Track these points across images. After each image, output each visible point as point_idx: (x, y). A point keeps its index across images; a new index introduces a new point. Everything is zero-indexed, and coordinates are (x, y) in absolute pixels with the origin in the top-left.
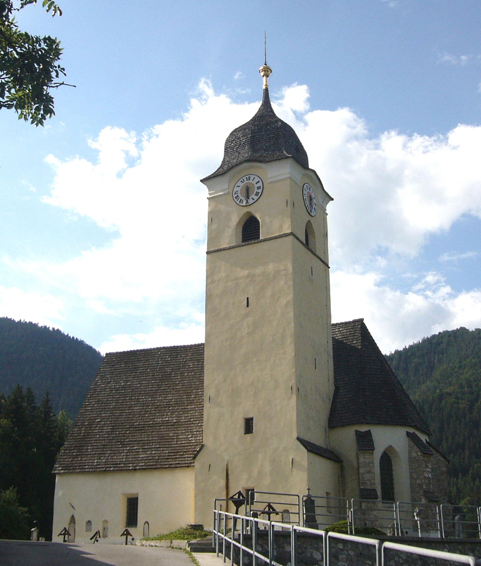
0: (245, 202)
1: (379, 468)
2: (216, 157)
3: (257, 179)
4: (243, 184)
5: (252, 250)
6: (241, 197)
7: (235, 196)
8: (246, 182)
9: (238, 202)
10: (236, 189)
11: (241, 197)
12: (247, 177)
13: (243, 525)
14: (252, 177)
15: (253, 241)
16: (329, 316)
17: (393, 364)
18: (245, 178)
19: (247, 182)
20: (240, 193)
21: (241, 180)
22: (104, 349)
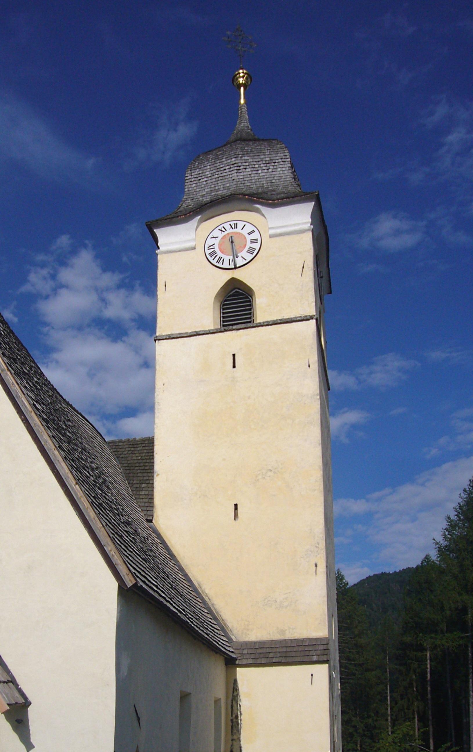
3: (249, 228)
4: (224, 234)
5: (237, 339)
7: (208, 252)
8: (229, 230)
9: (214, 262)
10: (210, 242)
14: (240, 225)
18: (227, 226)
21: (220, 228)
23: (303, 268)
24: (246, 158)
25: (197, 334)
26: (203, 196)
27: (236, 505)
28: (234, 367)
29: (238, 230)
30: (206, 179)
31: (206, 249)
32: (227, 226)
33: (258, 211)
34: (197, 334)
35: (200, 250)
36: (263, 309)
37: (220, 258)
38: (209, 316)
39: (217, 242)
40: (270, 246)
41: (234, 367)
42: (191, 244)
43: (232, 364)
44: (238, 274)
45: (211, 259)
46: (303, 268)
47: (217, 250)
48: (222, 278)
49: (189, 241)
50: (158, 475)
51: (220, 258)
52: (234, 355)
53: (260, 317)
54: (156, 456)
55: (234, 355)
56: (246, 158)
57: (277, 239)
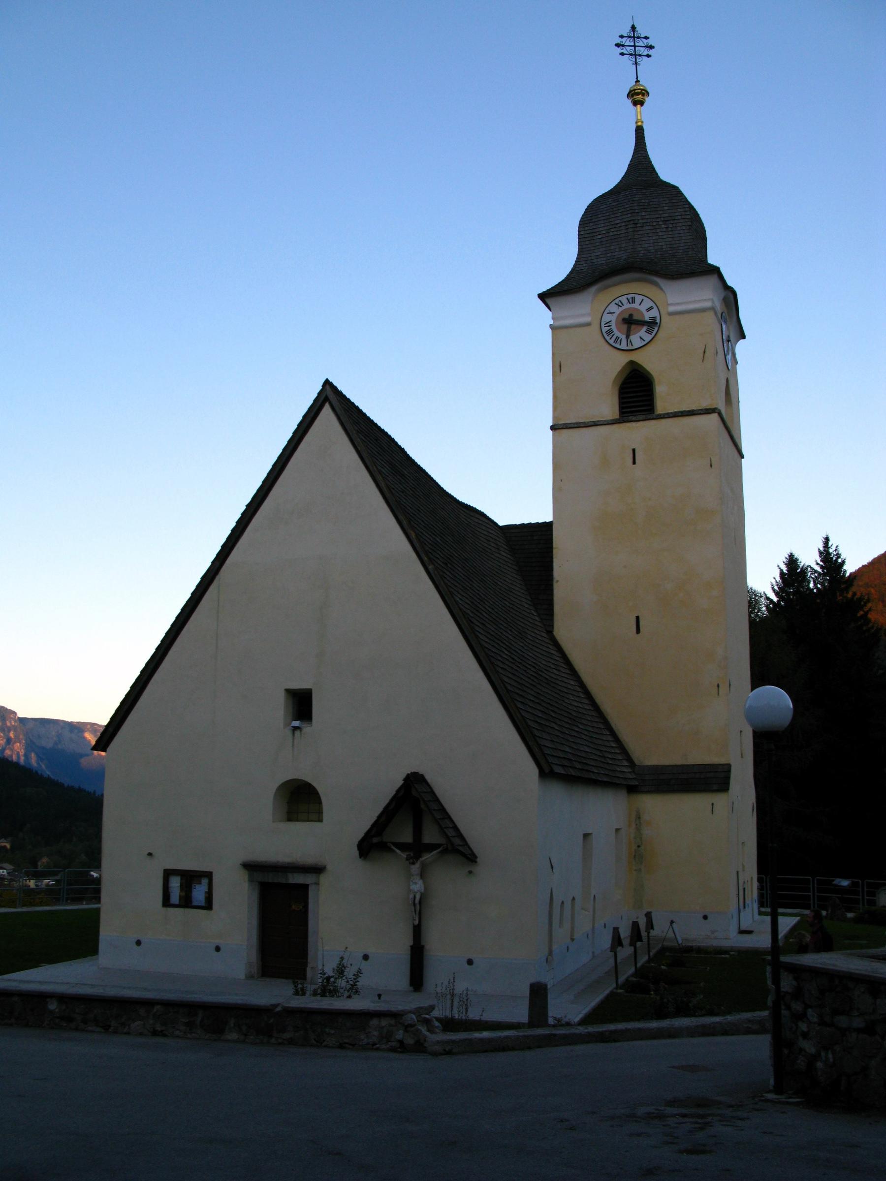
0: (624, 342)
1: (686, 1019)
2: (561, 259)
3: (647, 304)
4: (621, 309)
5: (638, 432)
6: (617, 333)
7: (605, 329)
8: (627, 306)
9: (611, 342)
10: (607, 318)
11: (617, 333)
12: (629, 296)
13: (725, 1031)
14: (638, 299)
15: (641, 417)
16: (409, 844)
17: (880, 615)
18: (624, 299)
19: (621, 309)
20: (616, 324)
21: (617, 301)
22: (501, 523)
23: (552, 868)
24: (643, 214)
25: (595, 424)
26: (597, 257)
27: (638, 618)
28: (634, 463)
29: (636, 305)
30: (600, 237)
31: (603, 326)
32: (624, 299)
33: (656, 285)
34: (595, 424)
35: (596, 326)
36: (665, 397)
37: (617, 338)
38: (609, 408)
39: (613, 318)
40: (668, 325)
41: (634, 463)
42: (587, 319)
43: (631, 460)
44: (637, 357)
45: (608, 338)
46: (552, 868)
47: (614, 328)
48: (620, 361)
49: (583, 315)
50: (557, 581)
51: (617, 338)
52: (634, 450)
53: (661, 407)
54: (555, 560)
55: (634, 450)
56: (643, 214)
57: (677, 317)
